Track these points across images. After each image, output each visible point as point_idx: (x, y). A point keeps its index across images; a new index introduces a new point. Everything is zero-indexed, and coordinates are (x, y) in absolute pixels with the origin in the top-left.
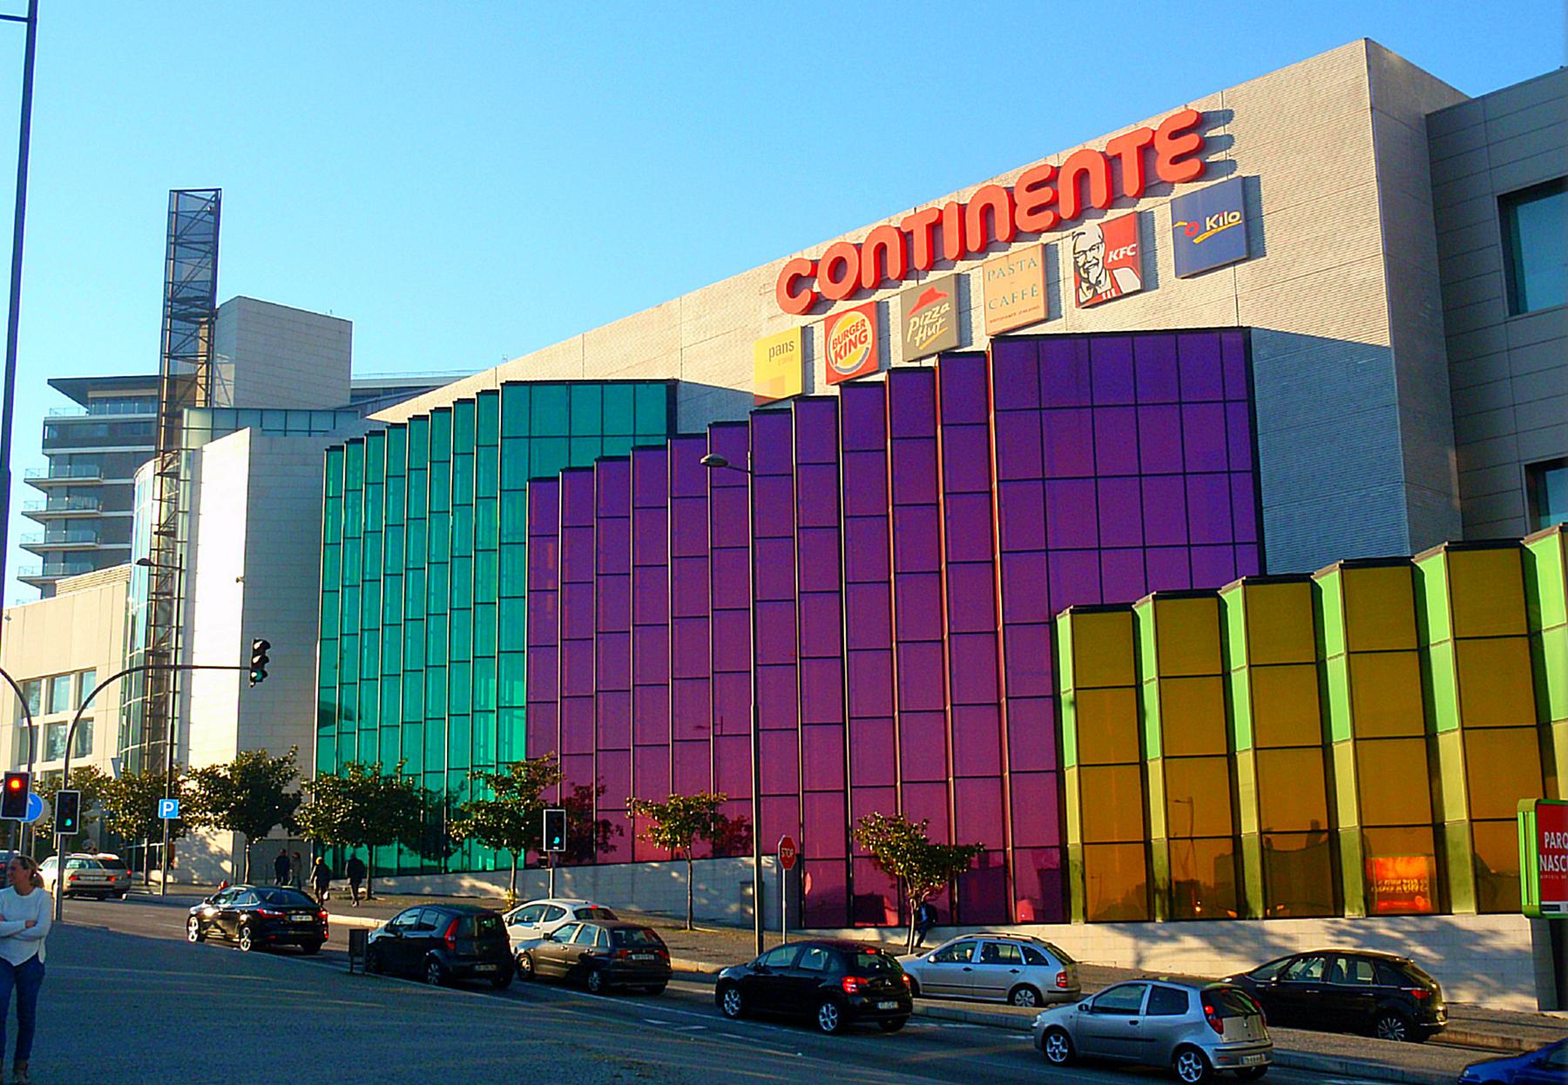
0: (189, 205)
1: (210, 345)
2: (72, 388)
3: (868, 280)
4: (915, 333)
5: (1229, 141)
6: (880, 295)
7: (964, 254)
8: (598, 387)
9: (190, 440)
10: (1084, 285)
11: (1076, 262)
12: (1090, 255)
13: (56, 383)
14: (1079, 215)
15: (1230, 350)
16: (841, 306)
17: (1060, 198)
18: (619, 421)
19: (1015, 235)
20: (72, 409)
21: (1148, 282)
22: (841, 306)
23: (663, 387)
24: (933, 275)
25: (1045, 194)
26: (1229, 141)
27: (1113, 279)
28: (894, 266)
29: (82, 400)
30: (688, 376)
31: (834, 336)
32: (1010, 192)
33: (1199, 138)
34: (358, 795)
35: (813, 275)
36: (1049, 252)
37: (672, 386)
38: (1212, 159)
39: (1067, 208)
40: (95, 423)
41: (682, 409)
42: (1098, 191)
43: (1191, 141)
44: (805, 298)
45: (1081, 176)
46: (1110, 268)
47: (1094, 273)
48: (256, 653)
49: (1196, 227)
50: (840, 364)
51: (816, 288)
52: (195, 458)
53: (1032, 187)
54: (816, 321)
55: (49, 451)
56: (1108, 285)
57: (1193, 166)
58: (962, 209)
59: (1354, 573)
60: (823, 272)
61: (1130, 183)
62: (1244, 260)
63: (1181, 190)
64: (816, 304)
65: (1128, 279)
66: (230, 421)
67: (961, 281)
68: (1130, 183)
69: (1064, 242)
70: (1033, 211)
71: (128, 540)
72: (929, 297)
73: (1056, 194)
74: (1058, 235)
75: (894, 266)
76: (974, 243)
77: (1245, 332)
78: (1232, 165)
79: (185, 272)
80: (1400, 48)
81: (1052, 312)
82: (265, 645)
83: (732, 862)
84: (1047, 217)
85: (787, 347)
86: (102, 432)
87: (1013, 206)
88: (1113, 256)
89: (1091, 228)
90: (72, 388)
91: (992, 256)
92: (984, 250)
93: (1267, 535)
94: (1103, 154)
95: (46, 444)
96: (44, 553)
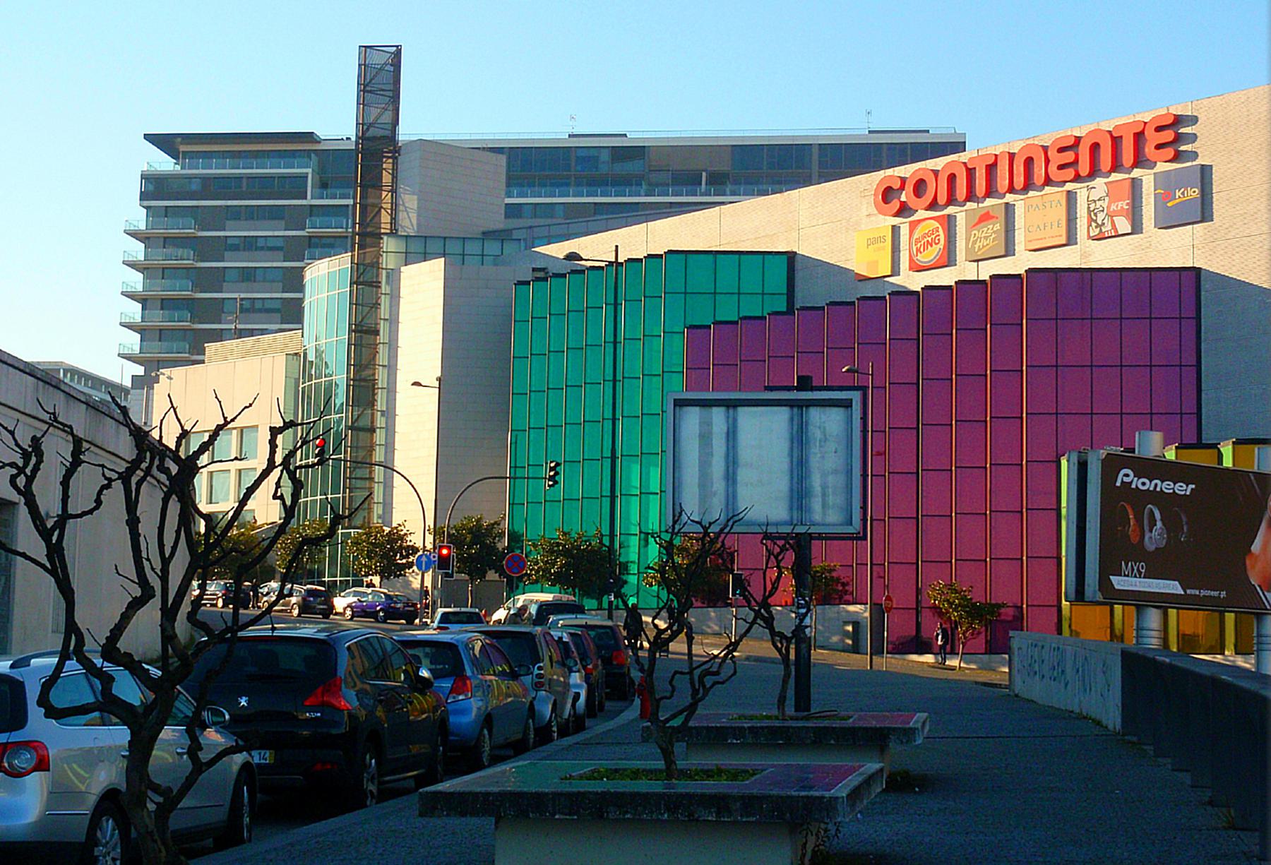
0: (377, 59)
1: (394, 177)
2: (163, 142)
3: (942, 199)
4: (974, 243)
5: (1193, 138)
6: (951, 210)
7: (1011, 189)
8: (737, 256)
9: (388, 261)
13: (152, 138)
14: (1093, 174)
15: (1189, 282)
16: (921, 214)
17: (1084, 158)
18: (751, 283)
19: (1048, 181)
20: (165, 163)
21: (1137, 228)
22: (921, 214)
23: (785, 257)
24: (989, 202)
25: (1069, 157)
26: (1193, 138)
27: (1113, 222)
29: (173, 153)
30: (803, 250)
31: (916, 236)
32: (1045, 149)
33: (1175, 134)
34: (567, 553)
35: (902, 188)
36: (1071, 196)
37: (791, 257)
38: (1182, 148)
39: (1084, 169)
40: (190, 178)
41: (799, 276)
43: (1168, 136)
44: (895, 205)
45: (1095, 147)
46: (1111, 216)
47: (1100, 217)
48: (551, 469)
49: (1169, 196)
51: (903, 198)
52: (394, 277)
53: (1061, 150)
54: (904, 223)
55: (146, 203)
57: (1169, 152)
58: (1012, 156)
59: (1237, 446)
60: (909, 188)
61: (1128, 156)
62: (1201, 222)
63: (1162, 167)
64: (903, 210)
65: (1124, 225)
66: (416, 247)
67: (1009, 208)
68: (1128, 156)
69: (1081, 190)
70: (1061, 167)
72: (986, 217)
73: (1077, 156)
74: (1079, 185)
77: (1197, 271)
78: (1195, 155)
82: (558, 464)
83: (835, 608)
84: (1070, 173)
85: (881, 239)
86: (195, 186)
87: (1047, 161)
89: (1099, 182)
90: (163, 142)
91: (1031, 193)
92: (1027, 187)
93: (1204, 410)
95: (144, 196)
96: (144, 301)
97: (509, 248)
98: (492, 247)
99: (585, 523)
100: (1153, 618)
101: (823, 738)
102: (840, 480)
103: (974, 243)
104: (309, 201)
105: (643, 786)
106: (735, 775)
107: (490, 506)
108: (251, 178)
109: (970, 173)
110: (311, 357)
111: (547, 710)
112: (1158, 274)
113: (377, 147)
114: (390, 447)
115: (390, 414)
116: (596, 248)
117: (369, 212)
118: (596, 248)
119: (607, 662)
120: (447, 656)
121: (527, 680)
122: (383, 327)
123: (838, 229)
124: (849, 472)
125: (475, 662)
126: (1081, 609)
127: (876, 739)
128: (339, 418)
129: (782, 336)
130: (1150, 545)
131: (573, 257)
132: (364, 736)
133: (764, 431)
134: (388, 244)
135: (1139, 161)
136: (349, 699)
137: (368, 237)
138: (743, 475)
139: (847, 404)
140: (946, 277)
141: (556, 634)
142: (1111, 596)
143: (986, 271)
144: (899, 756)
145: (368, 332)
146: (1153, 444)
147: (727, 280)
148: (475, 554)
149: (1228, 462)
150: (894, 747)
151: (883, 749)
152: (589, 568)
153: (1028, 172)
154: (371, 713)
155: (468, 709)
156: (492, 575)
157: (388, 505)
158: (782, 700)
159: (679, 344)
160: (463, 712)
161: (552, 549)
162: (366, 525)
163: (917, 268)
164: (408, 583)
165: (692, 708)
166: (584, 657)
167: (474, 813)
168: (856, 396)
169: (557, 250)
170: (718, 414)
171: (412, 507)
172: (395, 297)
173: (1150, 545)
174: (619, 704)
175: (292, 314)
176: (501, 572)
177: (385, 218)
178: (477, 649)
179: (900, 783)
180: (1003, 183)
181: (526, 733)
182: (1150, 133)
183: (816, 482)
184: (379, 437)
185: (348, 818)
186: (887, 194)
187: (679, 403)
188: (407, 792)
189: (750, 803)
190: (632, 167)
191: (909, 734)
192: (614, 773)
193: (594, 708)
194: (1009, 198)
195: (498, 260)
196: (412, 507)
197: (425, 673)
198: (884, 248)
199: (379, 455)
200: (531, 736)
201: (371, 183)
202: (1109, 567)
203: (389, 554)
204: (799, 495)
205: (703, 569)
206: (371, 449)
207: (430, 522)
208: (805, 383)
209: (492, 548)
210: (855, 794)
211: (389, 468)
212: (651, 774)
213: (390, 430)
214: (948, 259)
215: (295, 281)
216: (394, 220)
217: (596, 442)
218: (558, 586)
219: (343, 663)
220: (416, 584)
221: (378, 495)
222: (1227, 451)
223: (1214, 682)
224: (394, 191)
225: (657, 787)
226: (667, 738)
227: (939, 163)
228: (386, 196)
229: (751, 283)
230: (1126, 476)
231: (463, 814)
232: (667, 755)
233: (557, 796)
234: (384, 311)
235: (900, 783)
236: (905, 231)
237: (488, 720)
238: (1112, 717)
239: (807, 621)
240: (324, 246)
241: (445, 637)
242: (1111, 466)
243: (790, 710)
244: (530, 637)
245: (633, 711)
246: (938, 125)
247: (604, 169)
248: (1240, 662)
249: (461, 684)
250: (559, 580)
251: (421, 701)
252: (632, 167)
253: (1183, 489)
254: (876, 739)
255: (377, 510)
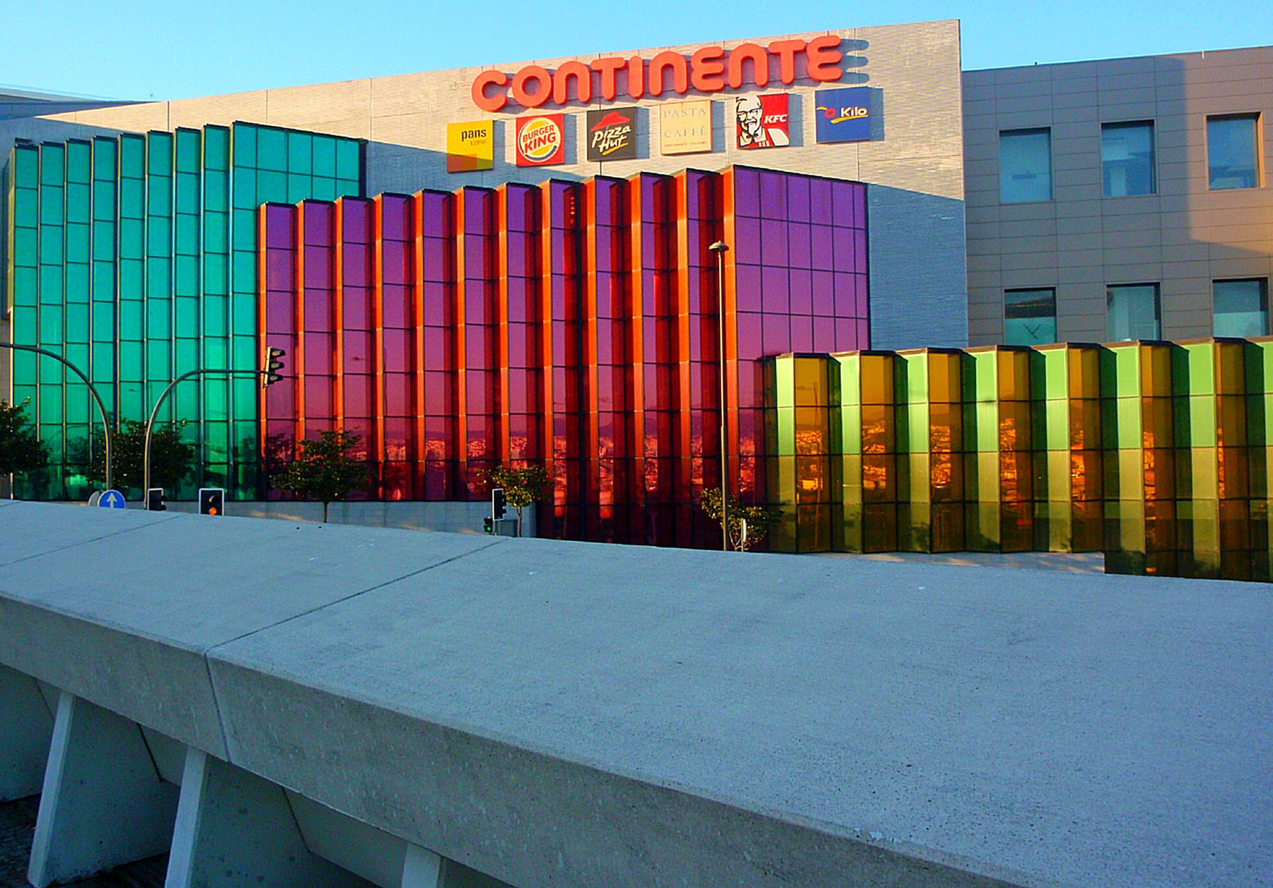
3: (560, 96)
4: (598, 143)
5: (863, 61)
10: (745, 135)
11: (738, 118)
12: (750, 116)
18: (324, 166)
19: (690, 89)
23: (356, 145)
25: (716, 67)
27: (767, 133)
37: (363, 144)
38: (849, 70)
41: (371, 164)
42: (583, 90)
46: (766, 126)
50: (529, 153)
51: (510, 94)
54: (509, 119)
56: (764, 138)
57: (835, 72)
69: (729, 102)
76: (655, 86)
81: (717, 145)
84: (718, 83)
88: (768, 119)
94: (766, 49)
103: (598, 143)
112: (817, 181)
147: (300, 162)
163: (594, 155)
182: (813, 52)
198: (483, 142)
218: (42, 448)
229: (324, 166)
236: (510, 128)
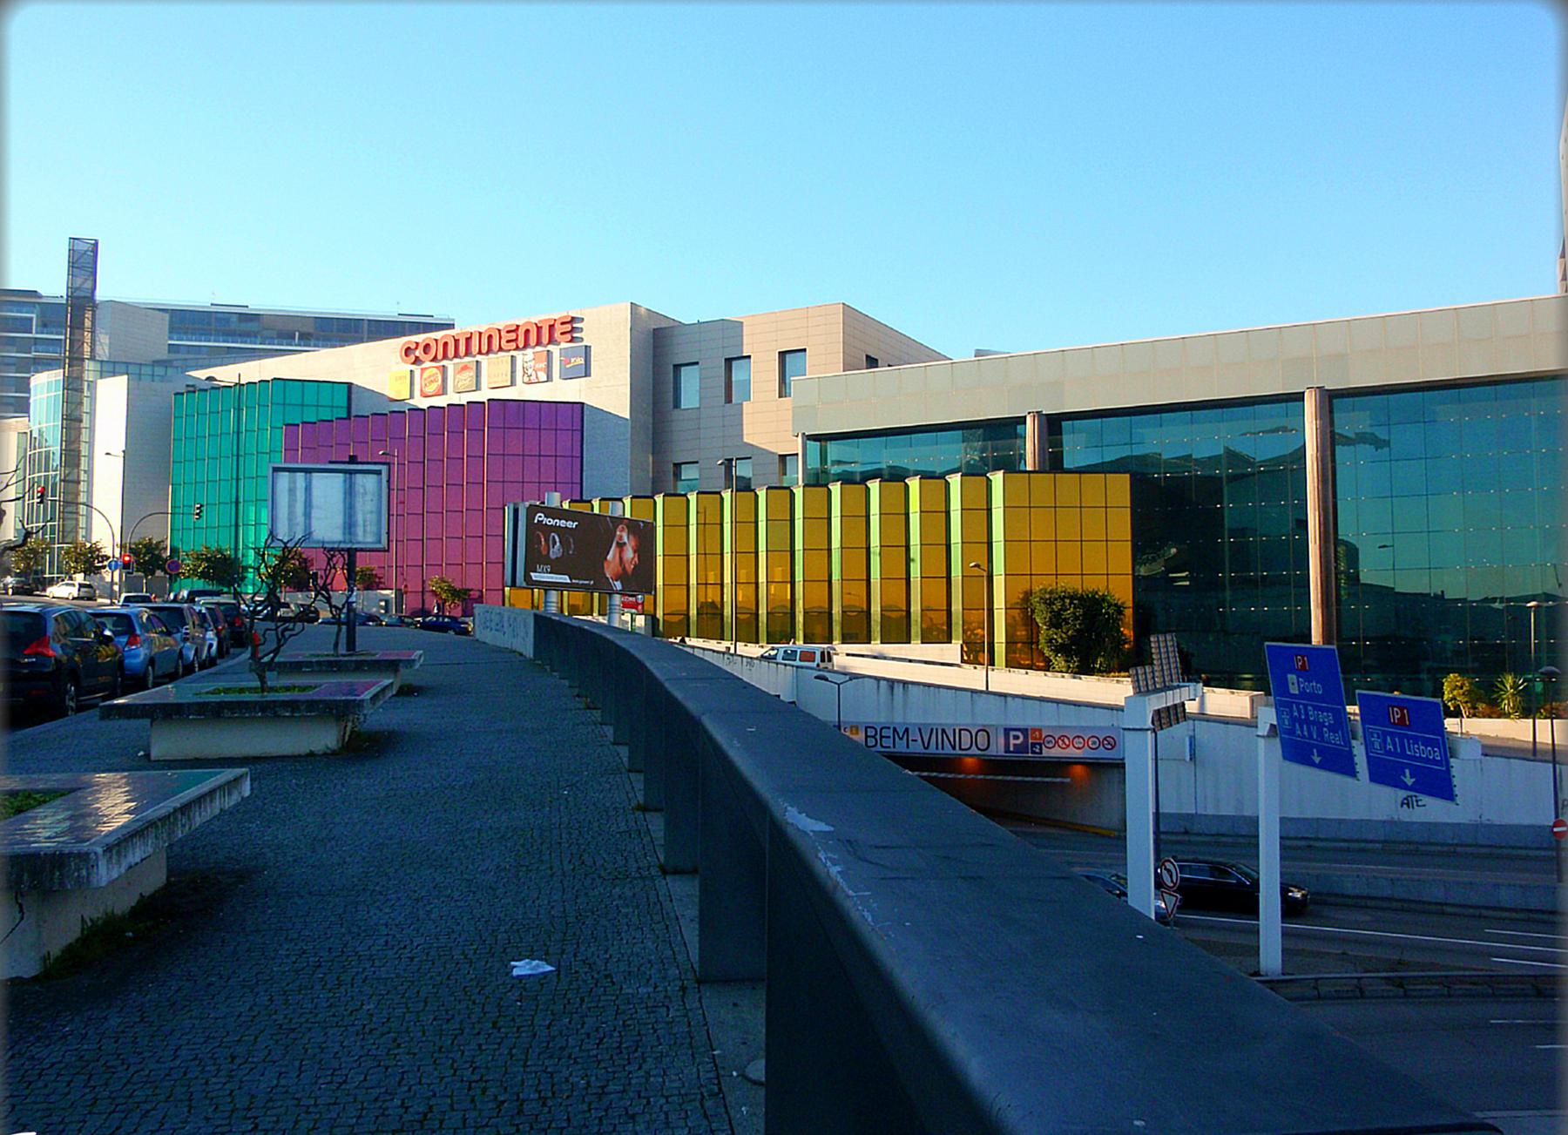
0: (81, 247)
3: (440, 356)
6: (444, 362)
7: (480, 352)
14: (526, 346)
16: (427, 364)
19: (501, 349)
21: (549, 379)
22: (427, 364)
24: (467, 359)
25: (513, 336)
28: (451, 352)
33: (572, 326)
34: (208, 560)
37: (350, 385)
43: (568, 328)
52: (92, 386)
57: (568, 337)
60: (421, 348)
61: (545, 339)
63: (564, 345)
64: (417, 361)
65: (543, 377)
68: (545, 339)
71: (1011, 664)
72: (465, 368)
75: (451, 352)
79: (78, 282)
80: (646, 304)
84: (513, 345)
89: (529, 351)
97: (170, 371)
98: (159, 371)
99: (220, 541)
100: (554, 596)
101: (359, 667)
102: (374, 516)
104: (33, 335)
105: (247, 697)
106: (304, 689)
107: (162, 532)
108: (15, 319)
109: (457, 341)
110: (35, 434)
111: (191, 654)
113: (81, 304)
114: (90, 493)
115: (90, 472)
116: (227, 374)
117: (76, 344)
118: (227, 374)
119: (231, 625)
120: (125, 623)
121: (178, 636)
122: (85, 417)
123: (378, 371)
124: (380, 512)
125: (142, 625)
126: (515, 591)
127: (392, 666)
128: (56, 473)
129: (343, 432)
130: (552, 556)
131: (210, 379)
132: (66, 672)
133: (328, 487)
134: (89, 365)
135: (551, 341)
136: (55, 650)
137: (76, 360)
138: (315, 513)
139: (379, 473)
140: (441, 402)
141: (197, 608)
142: (531, 584)
143: (463, 399)
144: (406, 676)
145: (74, 421)
146: (554, 499)
148: (146, 560)
149: (596, 511)
150: (403, 670)
151: (396, 671)
152: (223, 569)
153: (489, 343)
154: (71, 659)
155: (138, 655)
156: (159, 573)
157: (89, 529)
158: (336, 645)
159: (280, 435)
160: (137, 656)
161: (199, 557)
162: (74, 542)
164: (103, 579)
165: (276, 652)
166: (216, 622)
167: (137, 717)
168: (384, 468)
169: (201, 374)
170: (300, 475)
171: (105, 528)
172: (93, 399)
173: (552, 556)
174: (238, 650)
175: (23, 407)
176: (163, 570)
177: (87, 348)
178: (145, 617)
179: (406, 691)
180: (475, 349)
181: (177, 668)
183: (360, 518)
184: (83, 487)
185: (59, 722)
186: (408, 351)
187: (276, 470)
188: (96, 706)
189: (312, 705)
190: (252, 326)
191: (411, 663)
192: (227, 691)
193: (222, 653)
194: (479, 358)
195: (163, 378)
196: (105, 528)
197: (107, 633)
199: (82, 498)
200: (181, 670)
201: (77, 326)
202: (529, 568)
203: (90, 561)
204: (349, 525)
205: (294, 568)
206: (77, 494)
207: (118, 540)
208: (353, 460)
209: (159, 557)
210: (375, 697)
211: (89, 506)
212: (251, 690)
213: (90, 483)
214: (443, 391)
215: (24, 386)
216: (93, 350)
217: (226, 494)
219: (51, 628)
220: (108, 579)
221: (82, 523)
222: (596, 503)
223: (581, 629)
224: (93, 332)
225: (254, 697)
226: (261, 669)
227: (438, 335)
228: (87, 335)
229: (325, 401)
230: (540, 517)
231: (129, 718)
232: (262, 679)
233: (190, 705)
234: (86, 408)
235: (406, 691)
237: (151, 661)
238: (528, 651)
239: (353, 599)
240: (48, 364)
241: (124, 611)
242: (532, 511)
243: (342, 650)
244: (180, 610)
245: (247, 655)
246: (440, 315)
247: (233, 326)
248: (601, 620)
249: (133, 638)
250: (203, 575)
251: (110, 650)
252: (252, 326)
253: (572, 525)
254: (392, 666)
255: (82, 532)
